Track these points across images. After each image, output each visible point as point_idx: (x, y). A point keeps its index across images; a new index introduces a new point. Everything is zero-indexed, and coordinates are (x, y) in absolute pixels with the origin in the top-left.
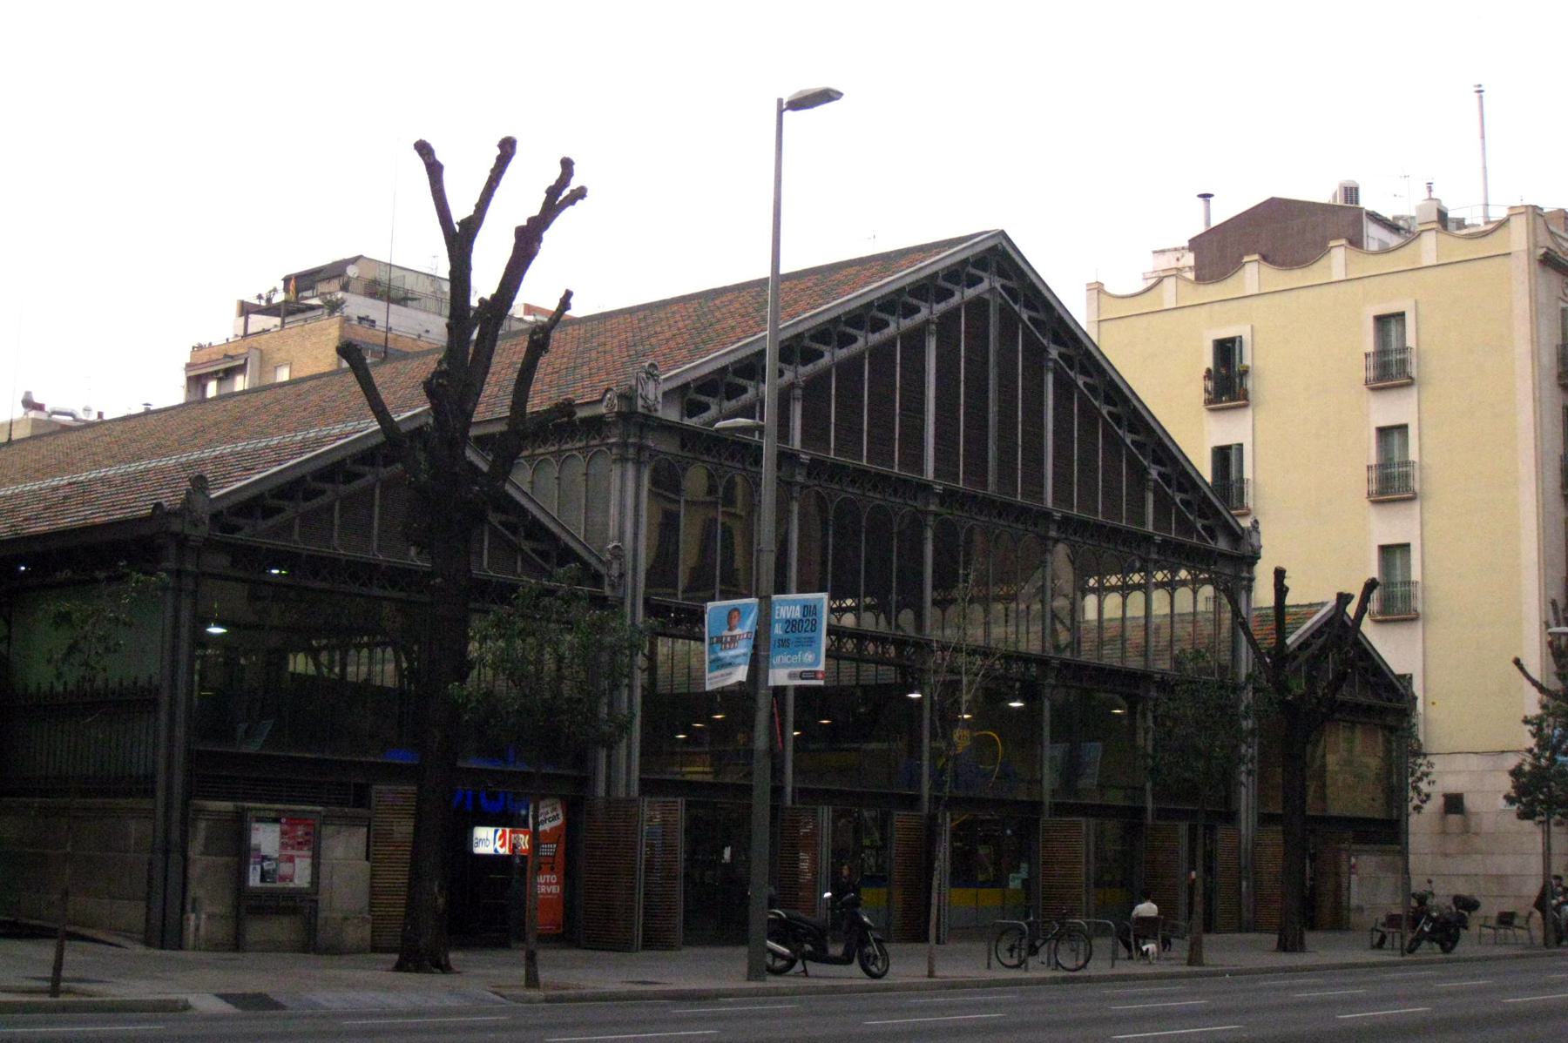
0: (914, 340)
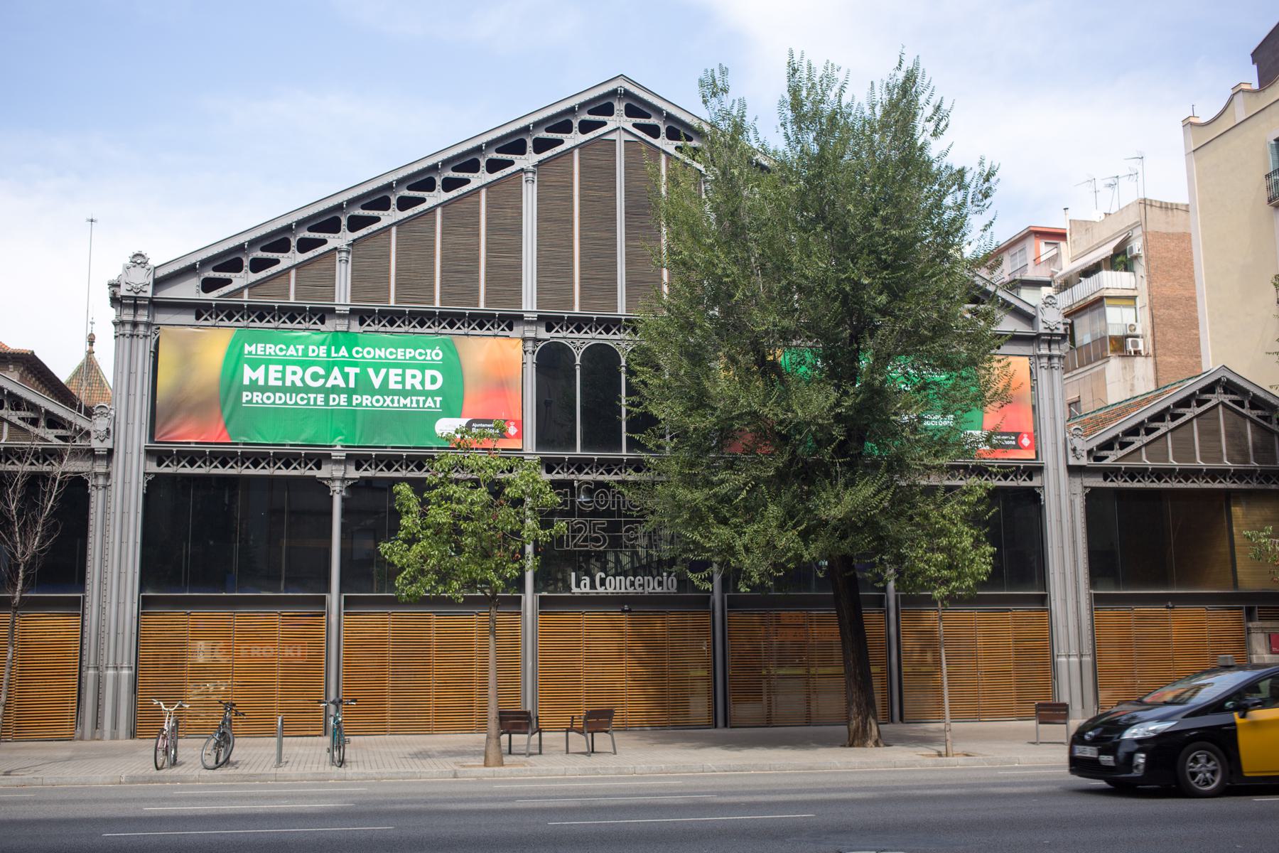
0: (505, 196)
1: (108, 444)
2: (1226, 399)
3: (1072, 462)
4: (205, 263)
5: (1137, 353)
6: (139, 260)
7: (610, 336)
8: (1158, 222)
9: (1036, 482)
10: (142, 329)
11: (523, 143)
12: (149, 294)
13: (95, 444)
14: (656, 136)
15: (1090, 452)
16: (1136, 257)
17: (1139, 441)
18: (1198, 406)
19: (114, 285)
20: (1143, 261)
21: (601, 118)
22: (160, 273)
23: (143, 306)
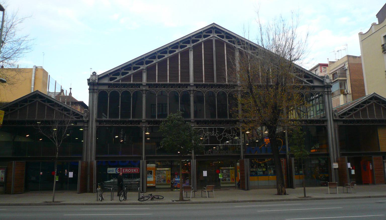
0: (185, 54)
1: (87, 119)
2: (375, 101)
3: (334, 118)
4: (110, 74)
5: (348, 93)
6: (94, 74)
7: (212, 89)
8: (352, 61)
9: (325, 124)
10: (95, 91)
11: (189, 41)
12: (97, 82)
13: (84, 119)
14: (223, 38)
15: (339, 116)
16: (347, 69)
17: (352, 113)
18: (354, 111)
19: (88, 80)
21: (209, 34)
22: (100, 77)
23: (96, 85)
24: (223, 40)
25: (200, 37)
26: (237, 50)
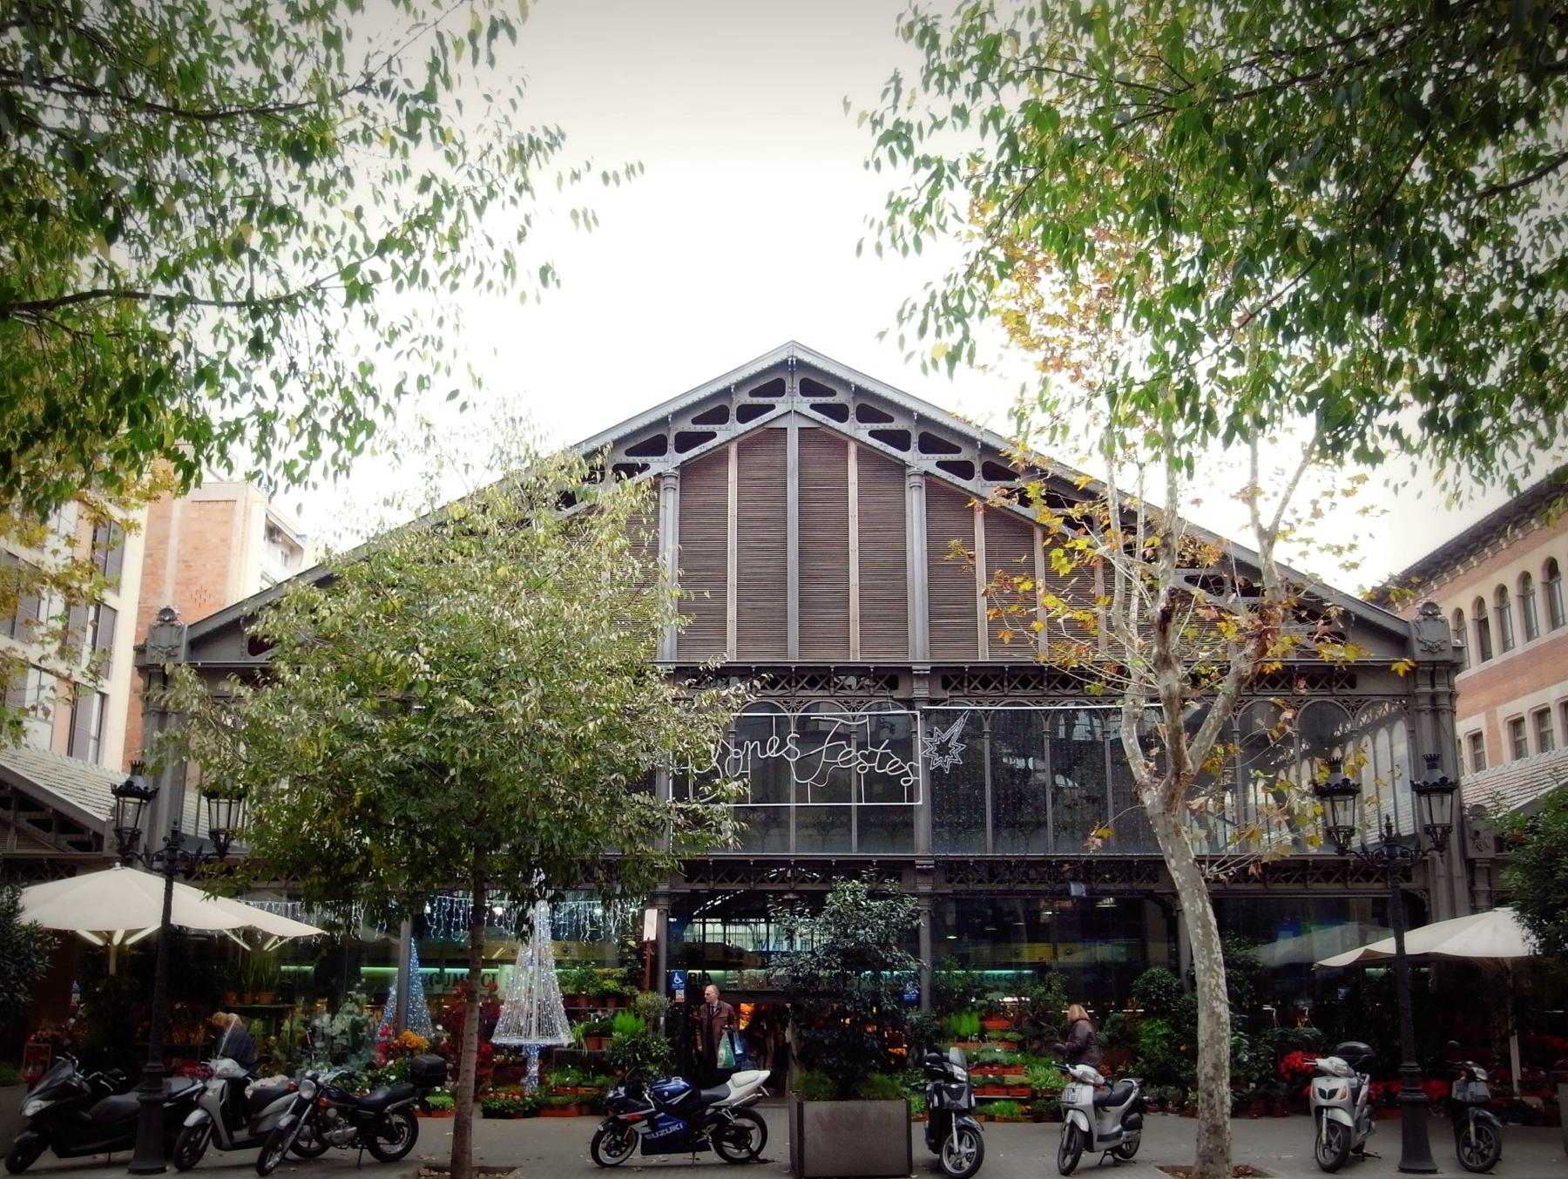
14: (905, 446)
20: (143, 532)
24: (843, 427)
25: (720, 416)
26: (915, 480)
